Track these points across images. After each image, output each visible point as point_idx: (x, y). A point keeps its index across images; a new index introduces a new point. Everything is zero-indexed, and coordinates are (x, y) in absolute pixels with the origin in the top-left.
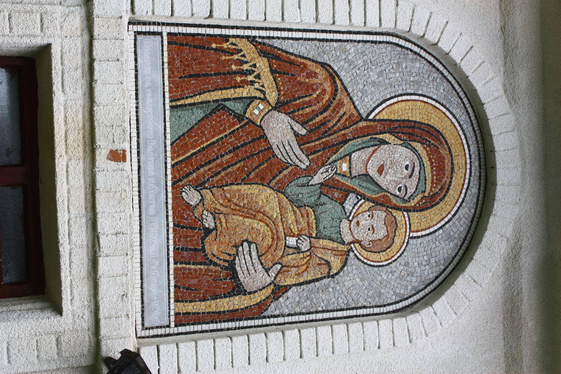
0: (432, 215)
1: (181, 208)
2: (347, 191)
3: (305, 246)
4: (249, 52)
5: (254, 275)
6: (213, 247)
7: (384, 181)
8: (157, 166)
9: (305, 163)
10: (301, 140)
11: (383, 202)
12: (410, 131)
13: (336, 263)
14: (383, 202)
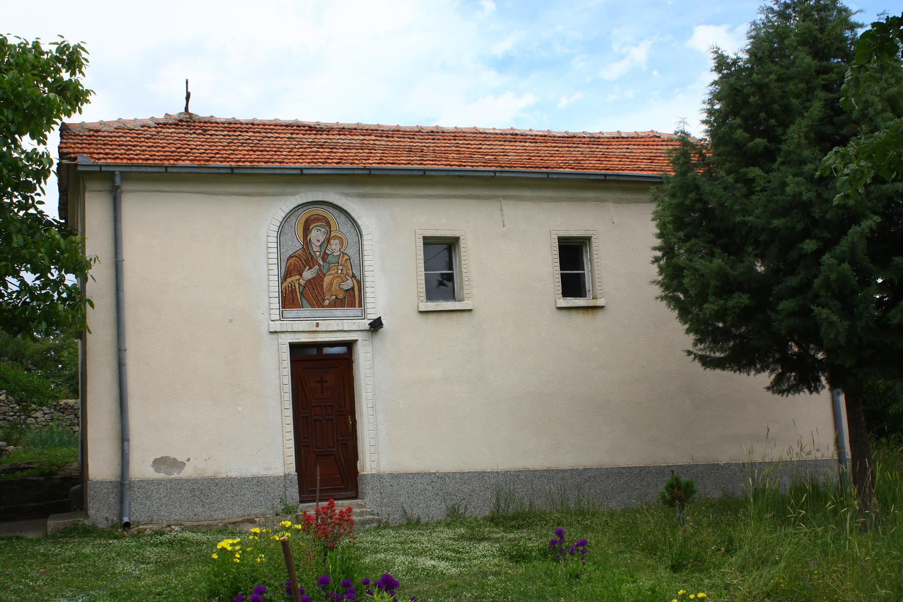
0: (332, 222)
2: (325, 252)
3: (341, 267)
4: (285, 284)
5: (348, 284)
6: (341, 296)
7: (322, 240)
8: (319, 312)
11: (328, 240)
12: (306, 231)
14: (328, 240)
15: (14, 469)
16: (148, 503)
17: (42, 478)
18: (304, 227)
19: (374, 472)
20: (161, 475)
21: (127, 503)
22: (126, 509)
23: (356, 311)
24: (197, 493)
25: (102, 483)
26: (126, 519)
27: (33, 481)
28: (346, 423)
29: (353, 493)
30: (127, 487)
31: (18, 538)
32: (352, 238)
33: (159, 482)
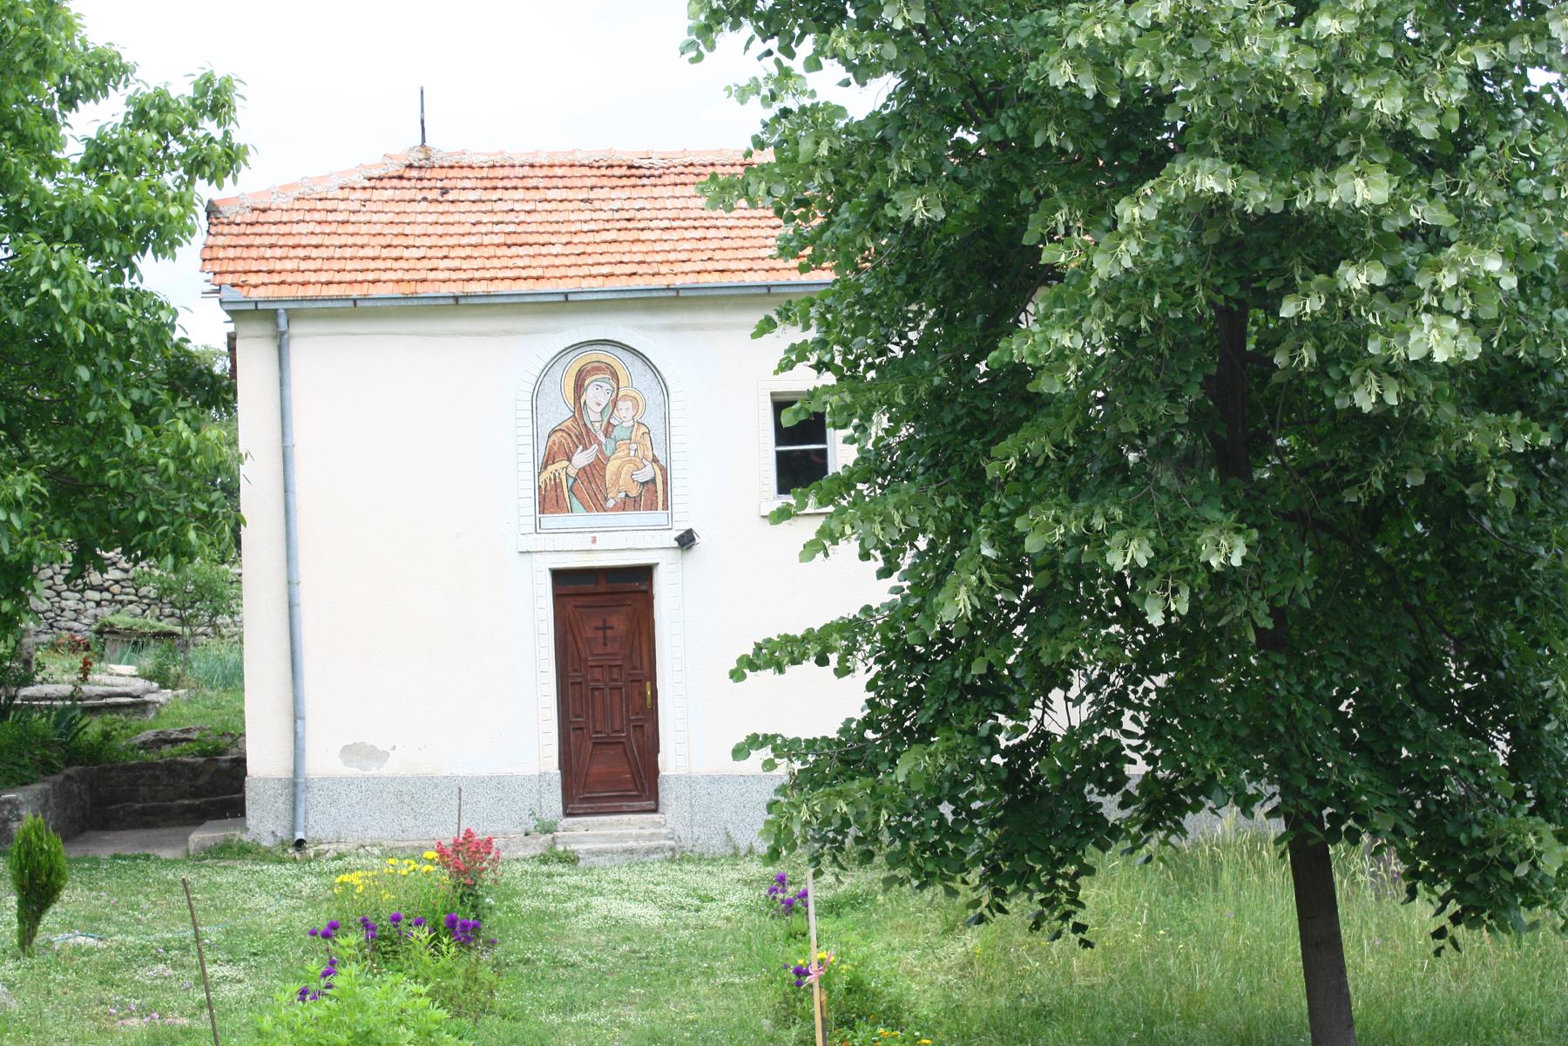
0: (621, 374)
1: (616, 508)
4: (545, 475)
5: (646, 473)
6: (634, 493)
9: (595, 446)
10: (585, 448)
12: (579, 387)
13: (643, 429)
15: (161, 741)
16: (334, 811)
17: (201, 760)
18: (576, 382)
19: (681, 772)
20: (352, 771)
21: (301, 810)
22: (301, 819)
23: (658, 517)
24: (407, 799)
25: (266, 780)
26: (300, 835)
27: (187, 764)
28: (643, 694)
29: (650, 804)
30: (301, 787)
31: (147, 857)
32: (653, 396)
33: (350, 782)
